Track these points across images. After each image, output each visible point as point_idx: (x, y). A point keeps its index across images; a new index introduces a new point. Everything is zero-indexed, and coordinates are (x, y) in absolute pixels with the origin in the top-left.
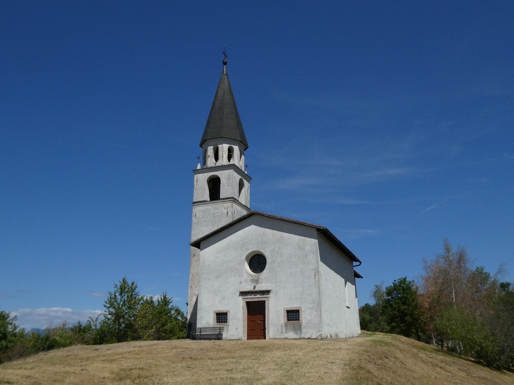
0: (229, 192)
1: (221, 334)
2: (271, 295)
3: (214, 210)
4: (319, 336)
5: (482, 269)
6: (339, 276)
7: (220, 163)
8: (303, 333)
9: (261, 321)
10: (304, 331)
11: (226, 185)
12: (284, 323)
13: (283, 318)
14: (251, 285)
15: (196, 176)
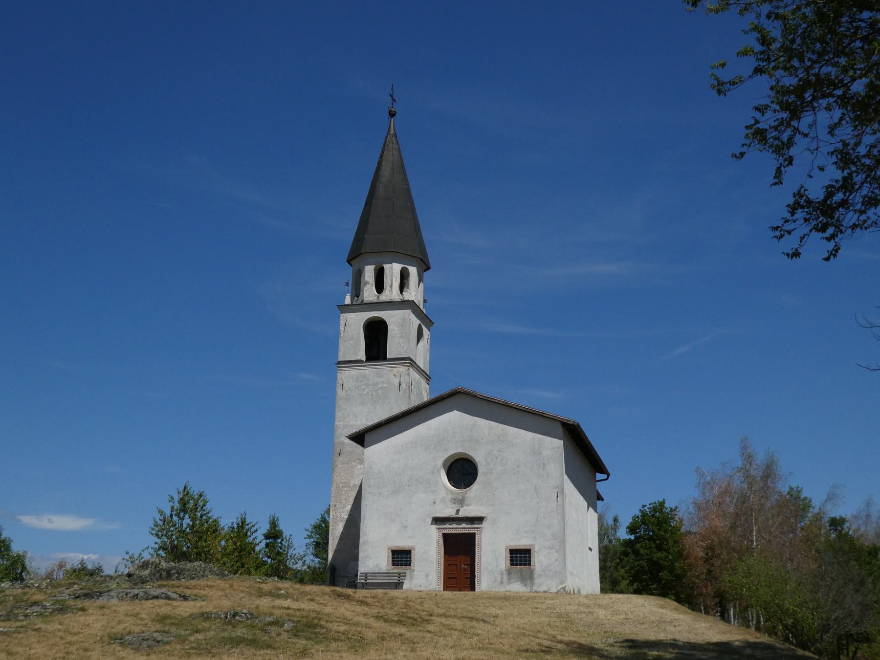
0: (403, 347)
1: (400, 584)
2: (485, 524)
3: (375, 378)
4: (562, 590)
5: (799, 492)
6: (582, 498)
7: (386, 296)
8: (536, 584)
9: (467, 565)
10: (537, 581)
12: (505, 568)
13: (503, 561)
14: (452, 508)
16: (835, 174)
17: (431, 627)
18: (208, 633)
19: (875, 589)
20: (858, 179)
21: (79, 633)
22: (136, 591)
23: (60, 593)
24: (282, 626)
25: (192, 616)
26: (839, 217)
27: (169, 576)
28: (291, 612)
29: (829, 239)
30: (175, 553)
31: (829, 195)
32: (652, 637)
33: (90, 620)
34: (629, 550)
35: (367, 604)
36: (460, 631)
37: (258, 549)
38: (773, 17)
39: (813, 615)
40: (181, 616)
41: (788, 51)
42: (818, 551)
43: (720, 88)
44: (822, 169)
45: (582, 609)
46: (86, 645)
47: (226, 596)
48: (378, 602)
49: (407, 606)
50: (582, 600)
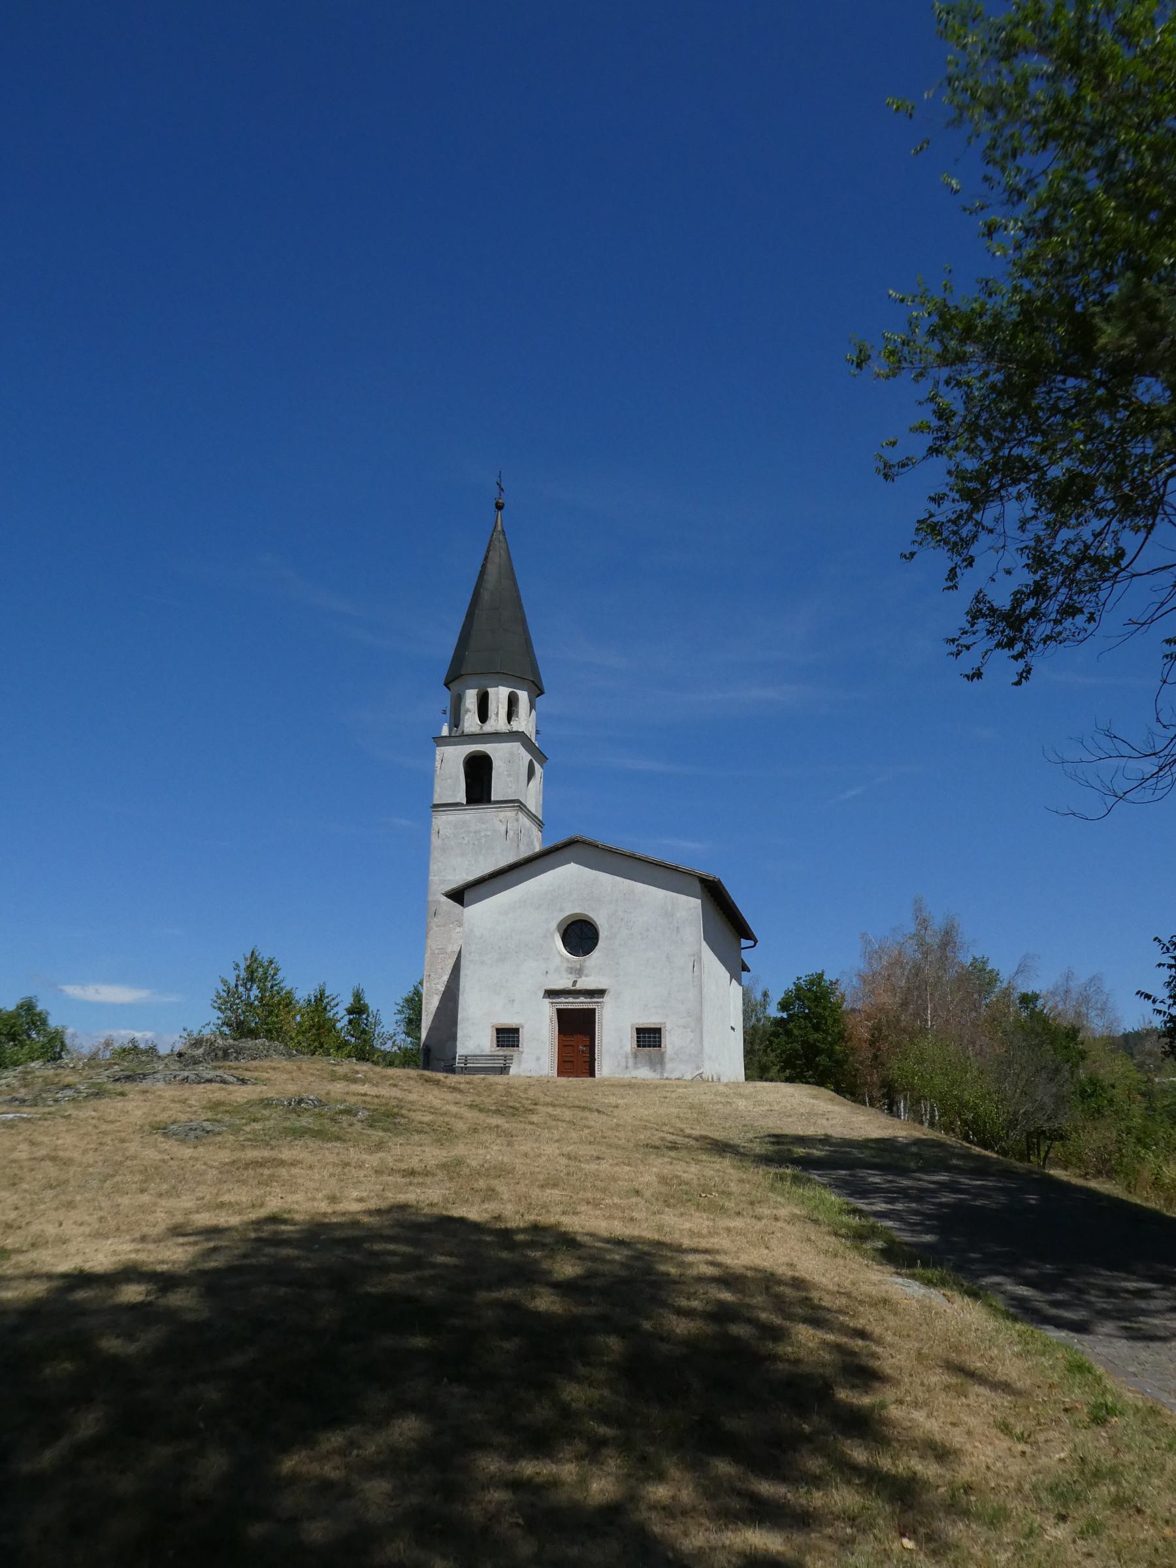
2: (607, 998)
10: (669, 1066)
11: (505, 773)
15: (440, 751)
16: (1027, 578)
17: (535, 1118)
18: (267, 1123)
19: (1072, 1078)
20: (1054, 581)
21: (117, 1121)
22: (186, 1074)
23: (97, 1074)
24: (355, 1115)
25: (250, 1103)
26: (1028, 630)
27: (226, 1055)
28: (368, 1099)
29: (1016, 658)
30: (241, 1030)
31: (1017, 602)
32: (800, 1132)
33: (130, 1106)
34: (781, 1030)
35: (460, 1091)
36: (569, 1122)
37: (339, 1025)
38: (952, 384)
39: (997, 1108)
40: (237, 1102)
41: (973, 428)
42: (1005, 1032)
43: (887, 473)
44: (1008, 572)
45: (719, 1099)
46: (123, 1134)
47: (292, 1080)
48: (474, 1088)
49: (508, 1093)
50: (721, 1089)
